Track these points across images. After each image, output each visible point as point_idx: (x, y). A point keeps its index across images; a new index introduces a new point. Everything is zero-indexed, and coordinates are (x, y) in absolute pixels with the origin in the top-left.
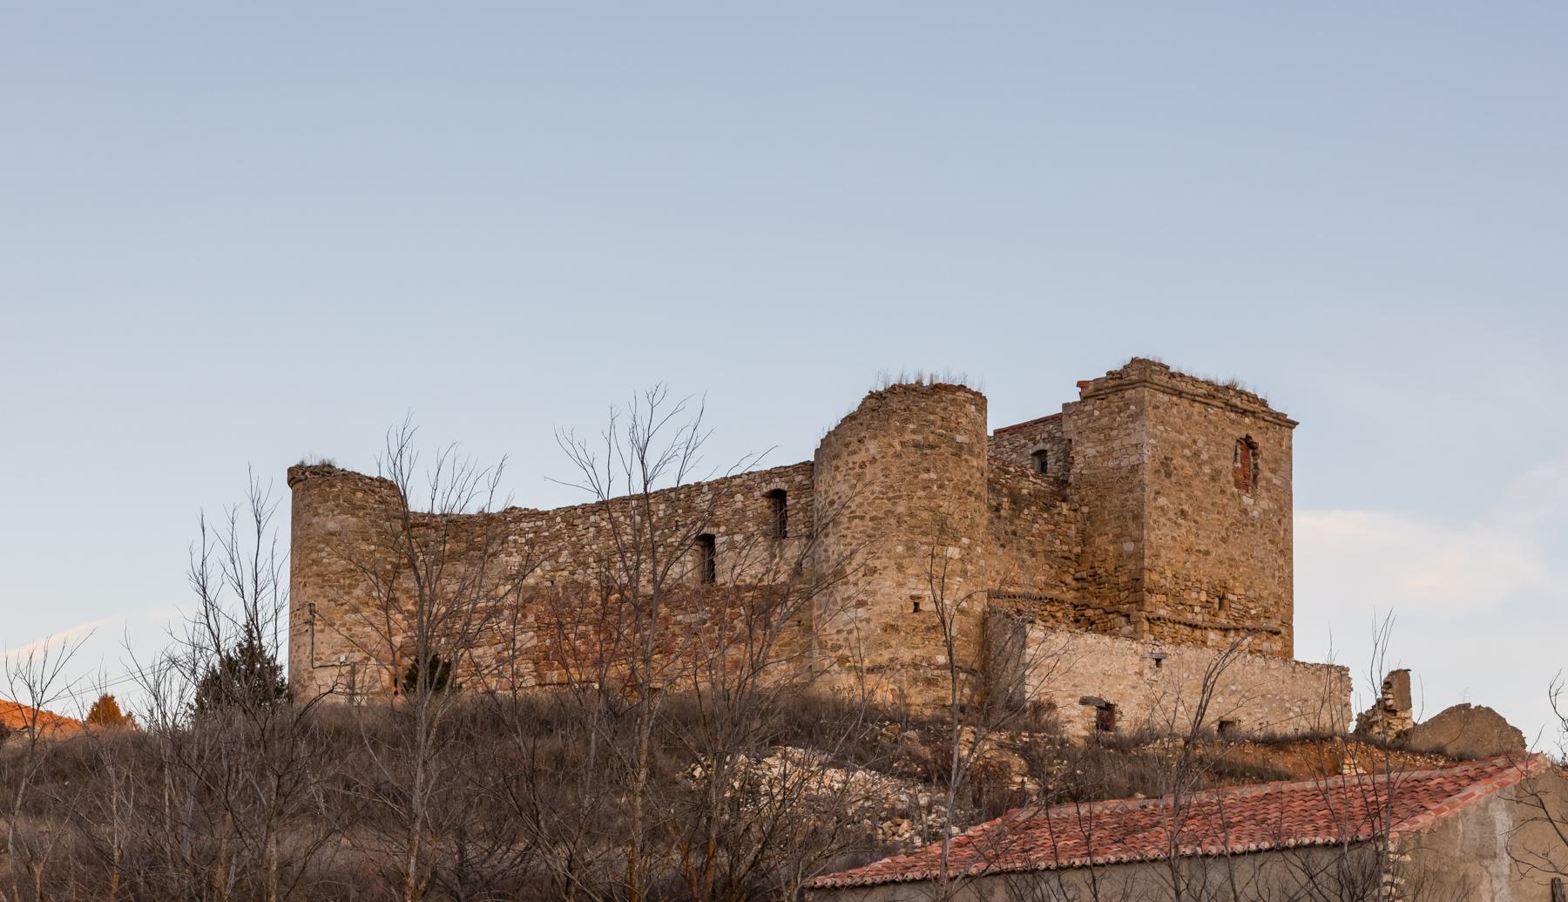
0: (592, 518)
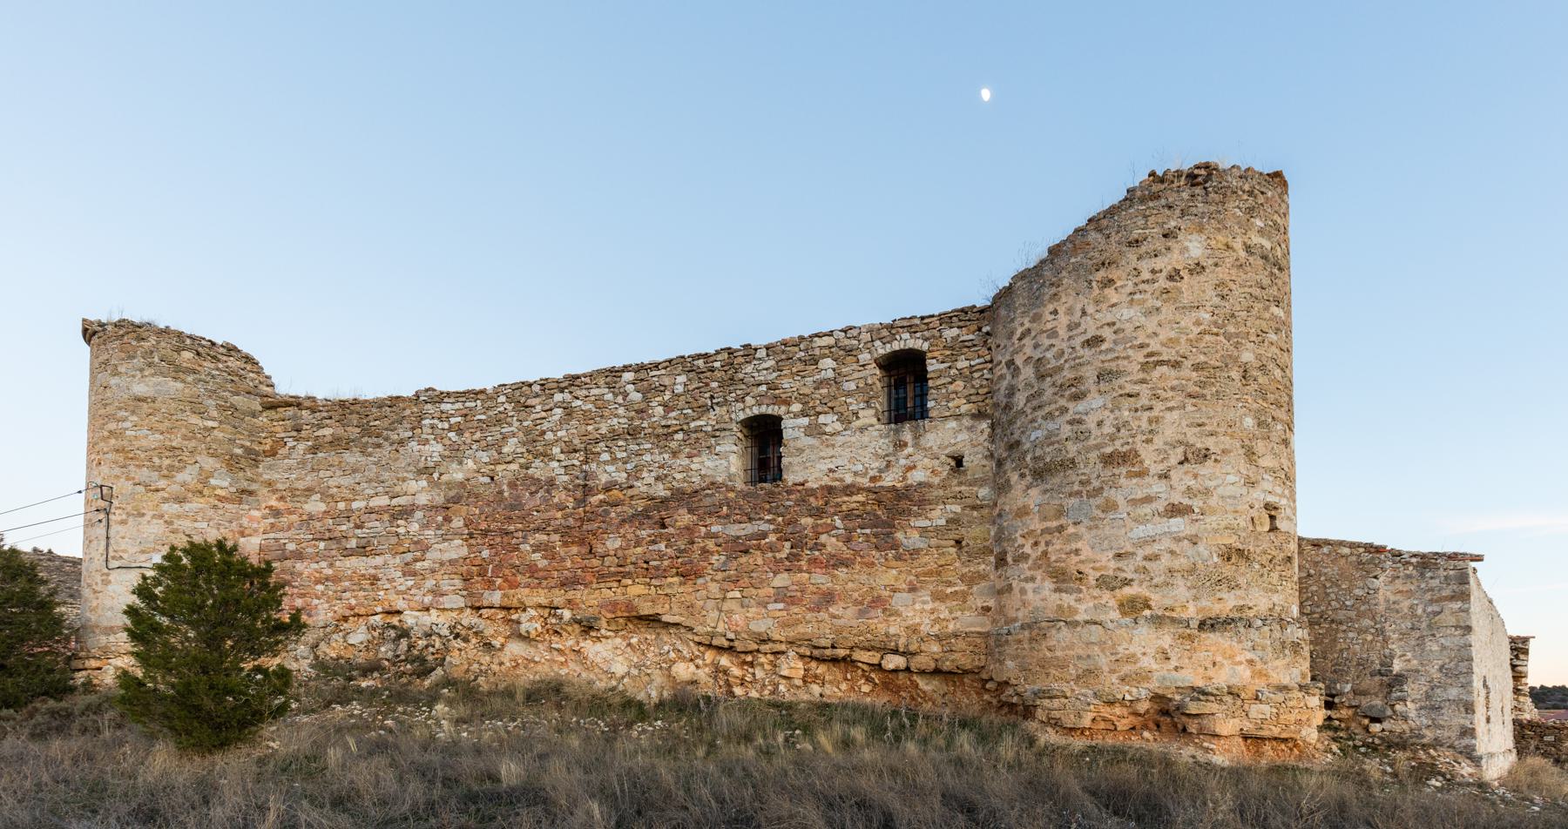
0: (558, 397)
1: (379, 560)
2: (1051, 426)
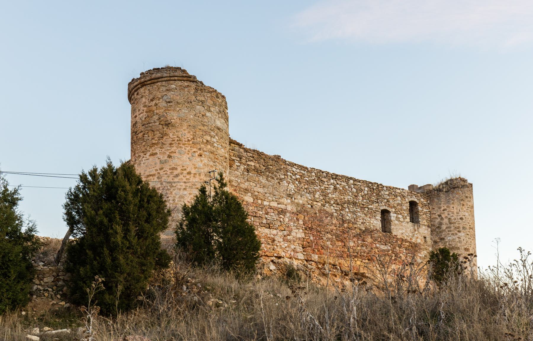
1: (275, 232)
2: (454, 237)
